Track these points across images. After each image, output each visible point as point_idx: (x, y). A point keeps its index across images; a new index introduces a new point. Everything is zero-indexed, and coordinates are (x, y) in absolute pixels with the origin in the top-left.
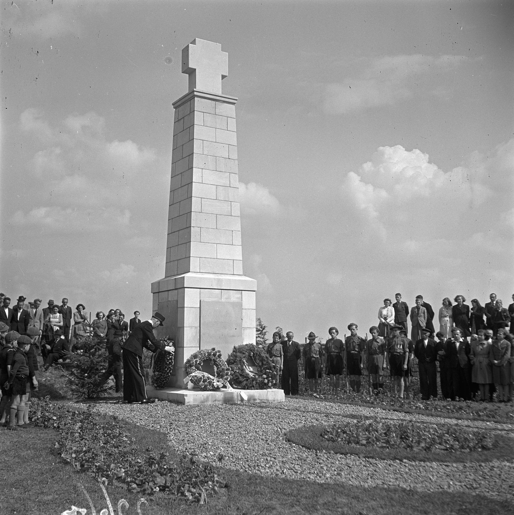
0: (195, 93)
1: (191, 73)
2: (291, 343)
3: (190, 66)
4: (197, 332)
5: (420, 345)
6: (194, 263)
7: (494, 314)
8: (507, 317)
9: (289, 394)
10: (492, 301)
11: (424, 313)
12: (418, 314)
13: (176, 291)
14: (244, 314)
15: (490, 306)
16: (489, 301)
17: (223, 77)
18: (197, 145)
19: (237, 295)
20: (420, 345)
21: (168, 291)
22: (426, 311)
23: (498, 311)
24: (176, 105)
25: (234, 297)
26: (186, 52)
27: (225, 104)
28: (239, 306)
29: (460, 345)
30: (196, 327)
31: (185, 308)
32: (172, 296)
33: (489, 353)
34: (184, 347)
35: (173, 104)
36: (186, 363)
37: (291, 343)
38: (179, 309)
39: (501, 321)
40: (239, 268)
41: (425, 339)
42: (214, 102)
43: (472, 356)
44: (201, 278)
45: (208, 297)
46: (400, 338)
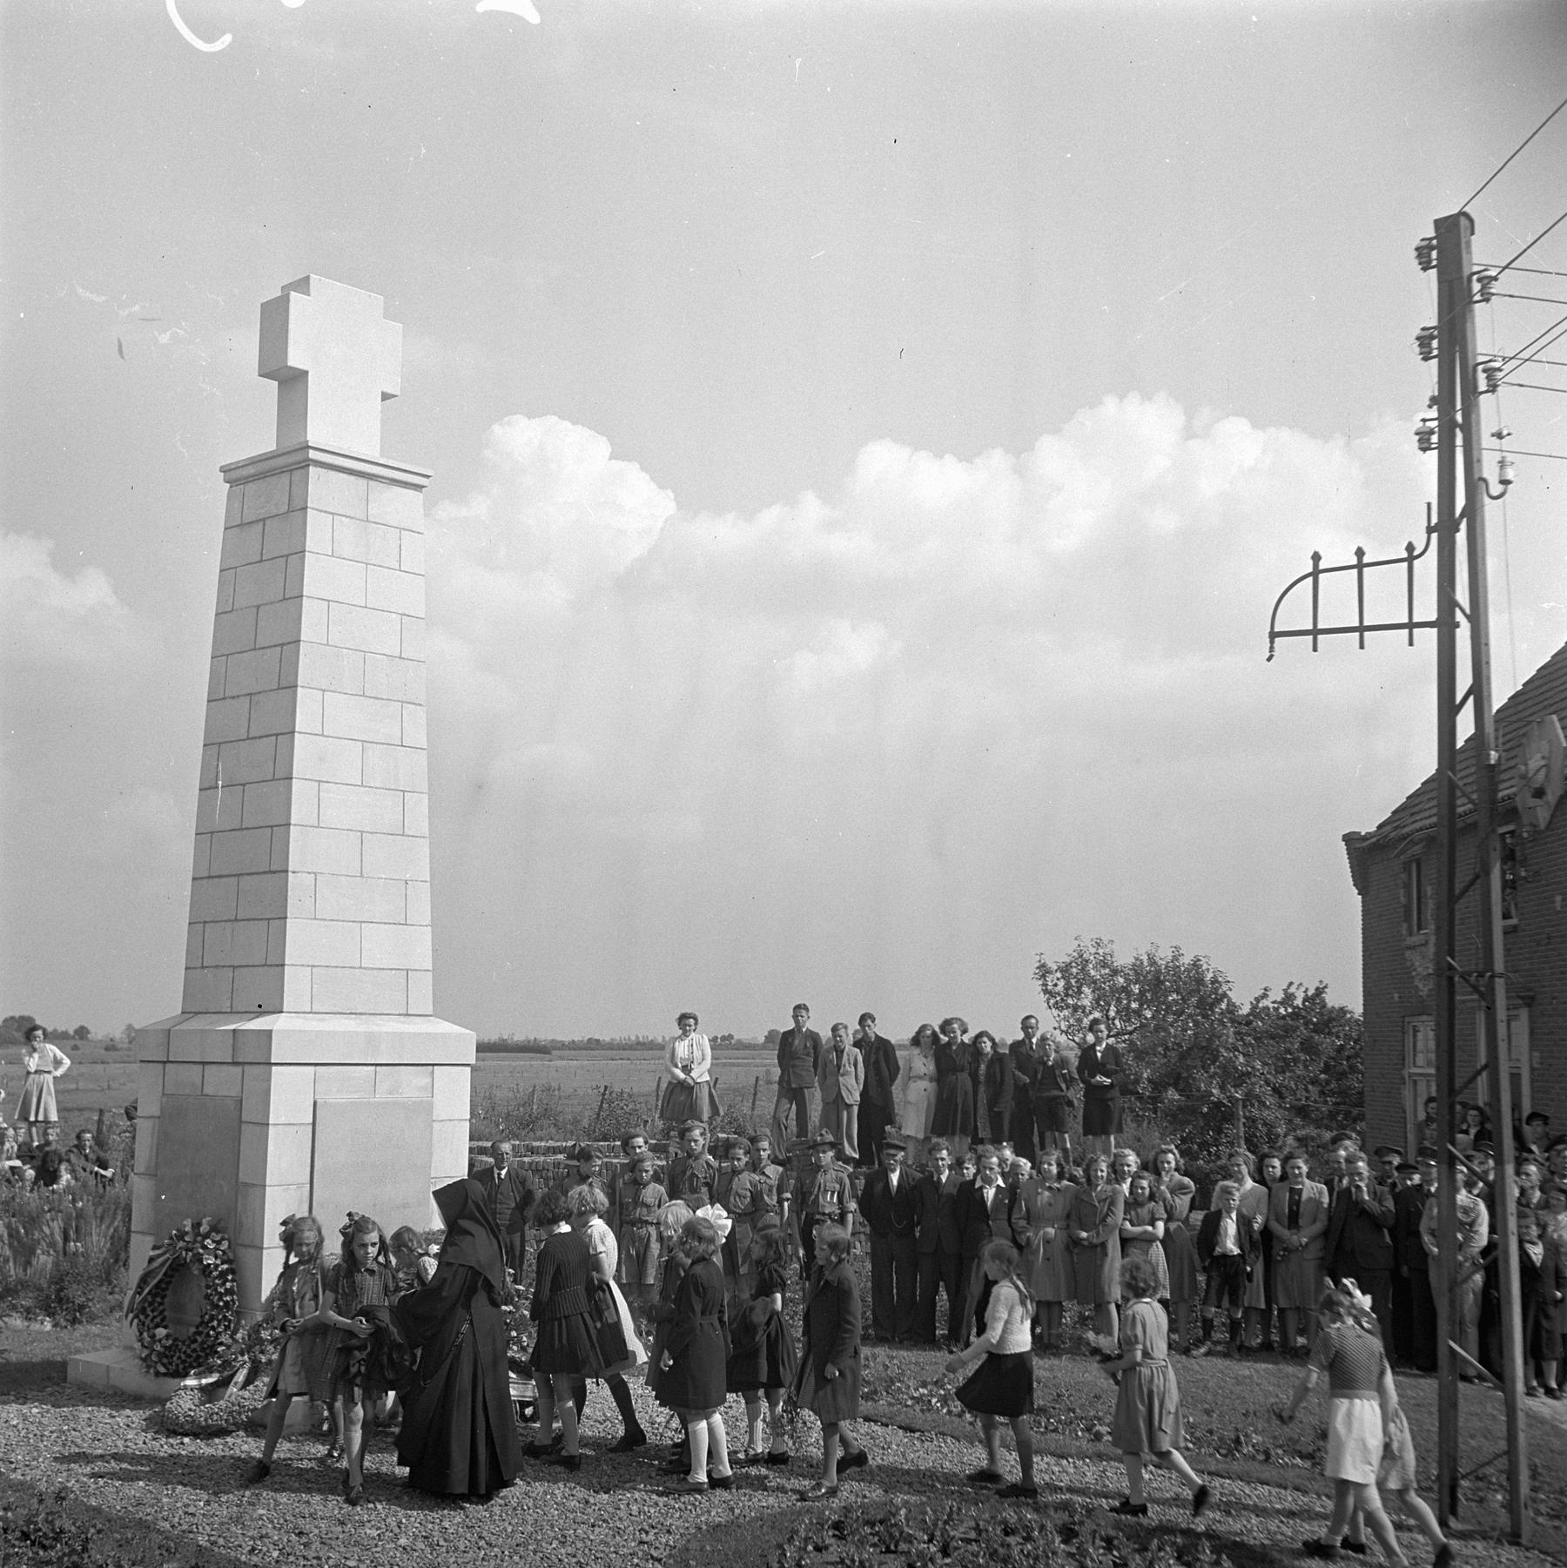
0: (312, 454)
1: (292, 383)
2: (504, 1172)
3: (291, 362)
4: (301, 1202)
5: (879, 1187)
6: (296, 984)
7: (1036, 1072)
8: (1070, 1081)
9: (173, 1113)
10: (1029, 1036)
11: (855, 1065)
12: (839, 1067)
13: (238, 1069)
14: (435, 1136)
15: (1023, 1050)
16: (1021, 1036)
17: (386, 397)
18: (311, 612)
19: (418, 1078)
20: (879, 1187)
21: (204, 1063)
22: (860, 1059)
23: (1045, 1064)
24: (233, 475)
25: (413, 1081)
26: (274, 318)
27: (397, 490)
28: (424, 1109)
29: (996, 1194)
30: (299, 1186)
31: (271, 1130)
32: (220, 1082)
33: (1068, 1216)
34: (262, 1248)
35: (225, 470)
36: (271, 1300)
37: (504, 1172)
38: (244, 1127)
39: (1056, 1093)
40: (423, 994)
41: (893, 1171)
42: (362, 482)
43: (1023, 1223)
44: (319, 1034)
45: (339, 1089)
46: (832, 1174)
